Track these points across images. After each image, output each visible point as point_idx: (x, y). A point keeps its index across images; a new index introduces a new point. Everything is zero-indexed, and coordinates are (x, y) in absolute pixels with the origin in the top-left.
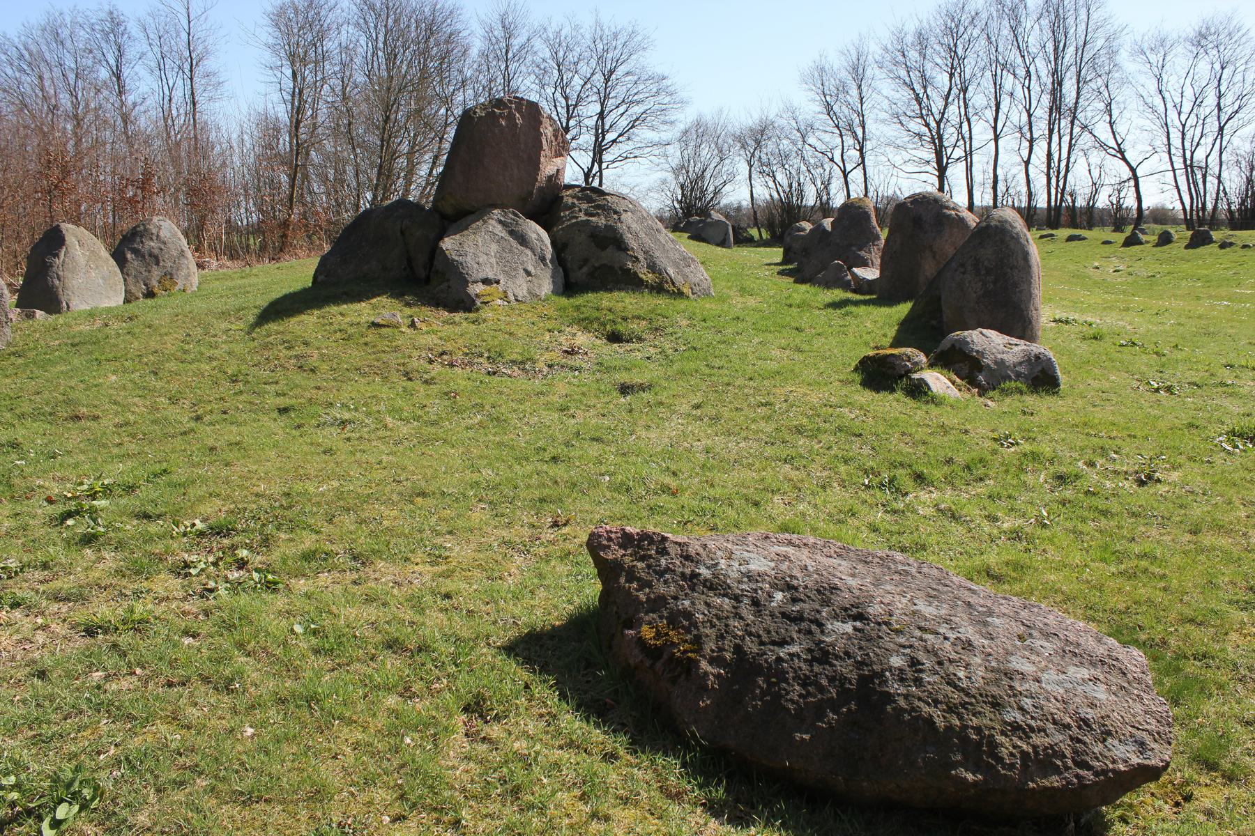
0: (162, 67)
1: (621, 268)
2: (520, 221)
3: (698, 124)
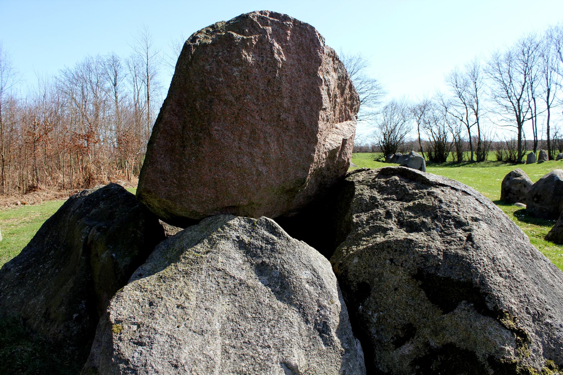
0: (135, 80)
1: (492, 360)
2: (280, 243)
3: (392, 104)
